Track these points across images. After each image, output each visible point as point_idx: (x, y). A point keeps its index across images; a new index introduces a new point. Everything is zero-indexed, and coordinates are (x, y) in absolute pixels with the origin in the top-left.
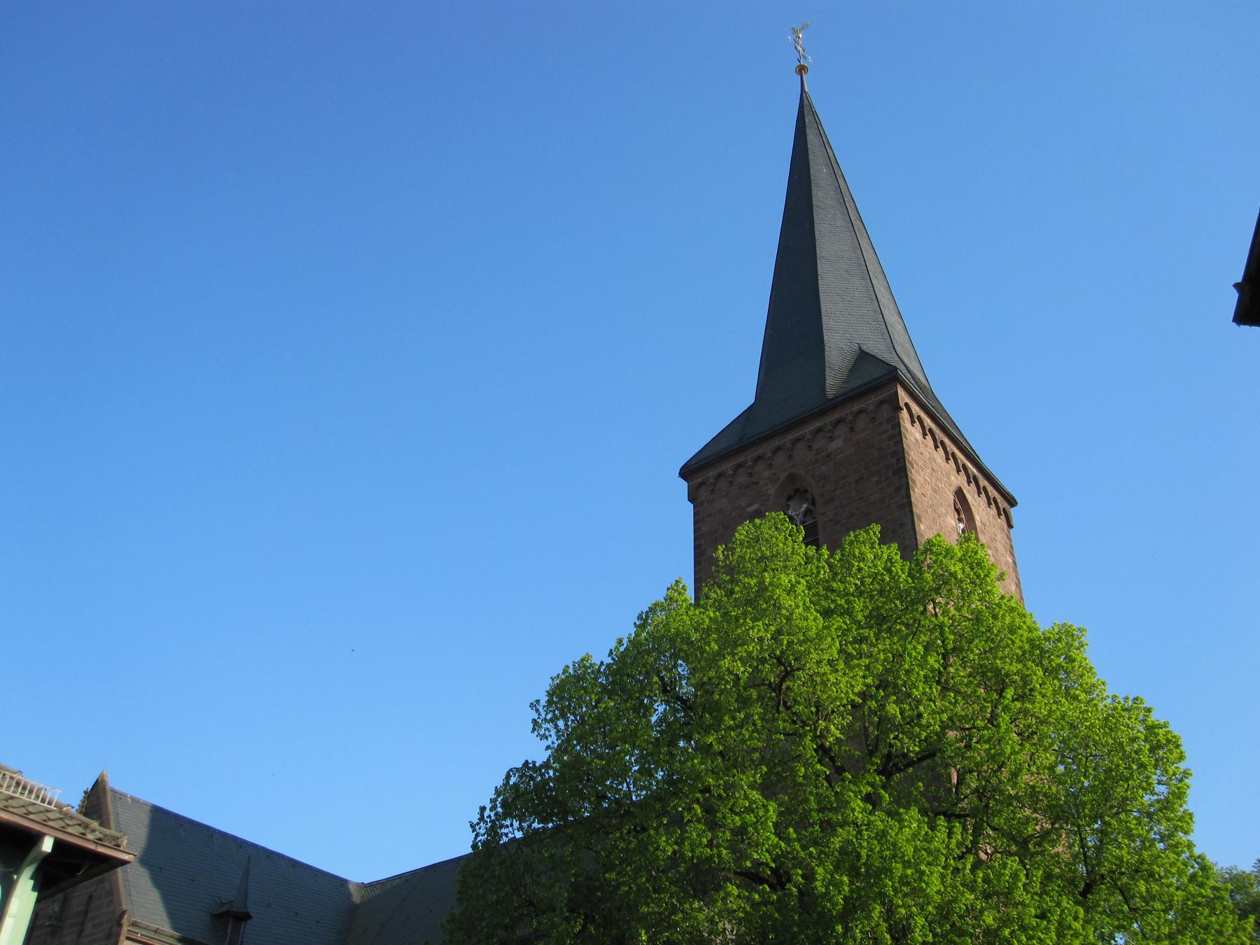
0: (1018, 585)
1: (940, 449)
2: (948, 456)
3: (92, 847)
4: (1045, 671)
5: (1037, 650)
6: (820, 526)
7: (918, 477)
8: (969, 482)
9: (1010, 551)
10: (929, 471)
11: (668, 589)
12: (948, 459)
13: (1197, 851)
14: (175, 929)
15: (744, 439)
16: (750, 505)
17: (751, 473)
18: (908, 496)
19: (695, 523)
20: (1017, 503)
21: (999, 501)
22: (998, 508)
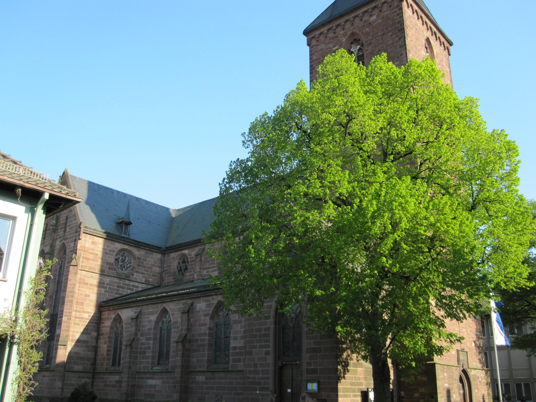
0: (451, 81)
1: (420, 20)
3: (65, 196)
4: (461, 117)
5: (457, 108)
6: (365, 56)
7: (409, 33)
10: (414, 30)
11: (298, 84)
12: (423, 24)
13: (519, 193)
14: (102, 228)
16: (334, 47)
17: (335, 32)
18: (405, 41)
19: (310, 55)
22: (444, 46)
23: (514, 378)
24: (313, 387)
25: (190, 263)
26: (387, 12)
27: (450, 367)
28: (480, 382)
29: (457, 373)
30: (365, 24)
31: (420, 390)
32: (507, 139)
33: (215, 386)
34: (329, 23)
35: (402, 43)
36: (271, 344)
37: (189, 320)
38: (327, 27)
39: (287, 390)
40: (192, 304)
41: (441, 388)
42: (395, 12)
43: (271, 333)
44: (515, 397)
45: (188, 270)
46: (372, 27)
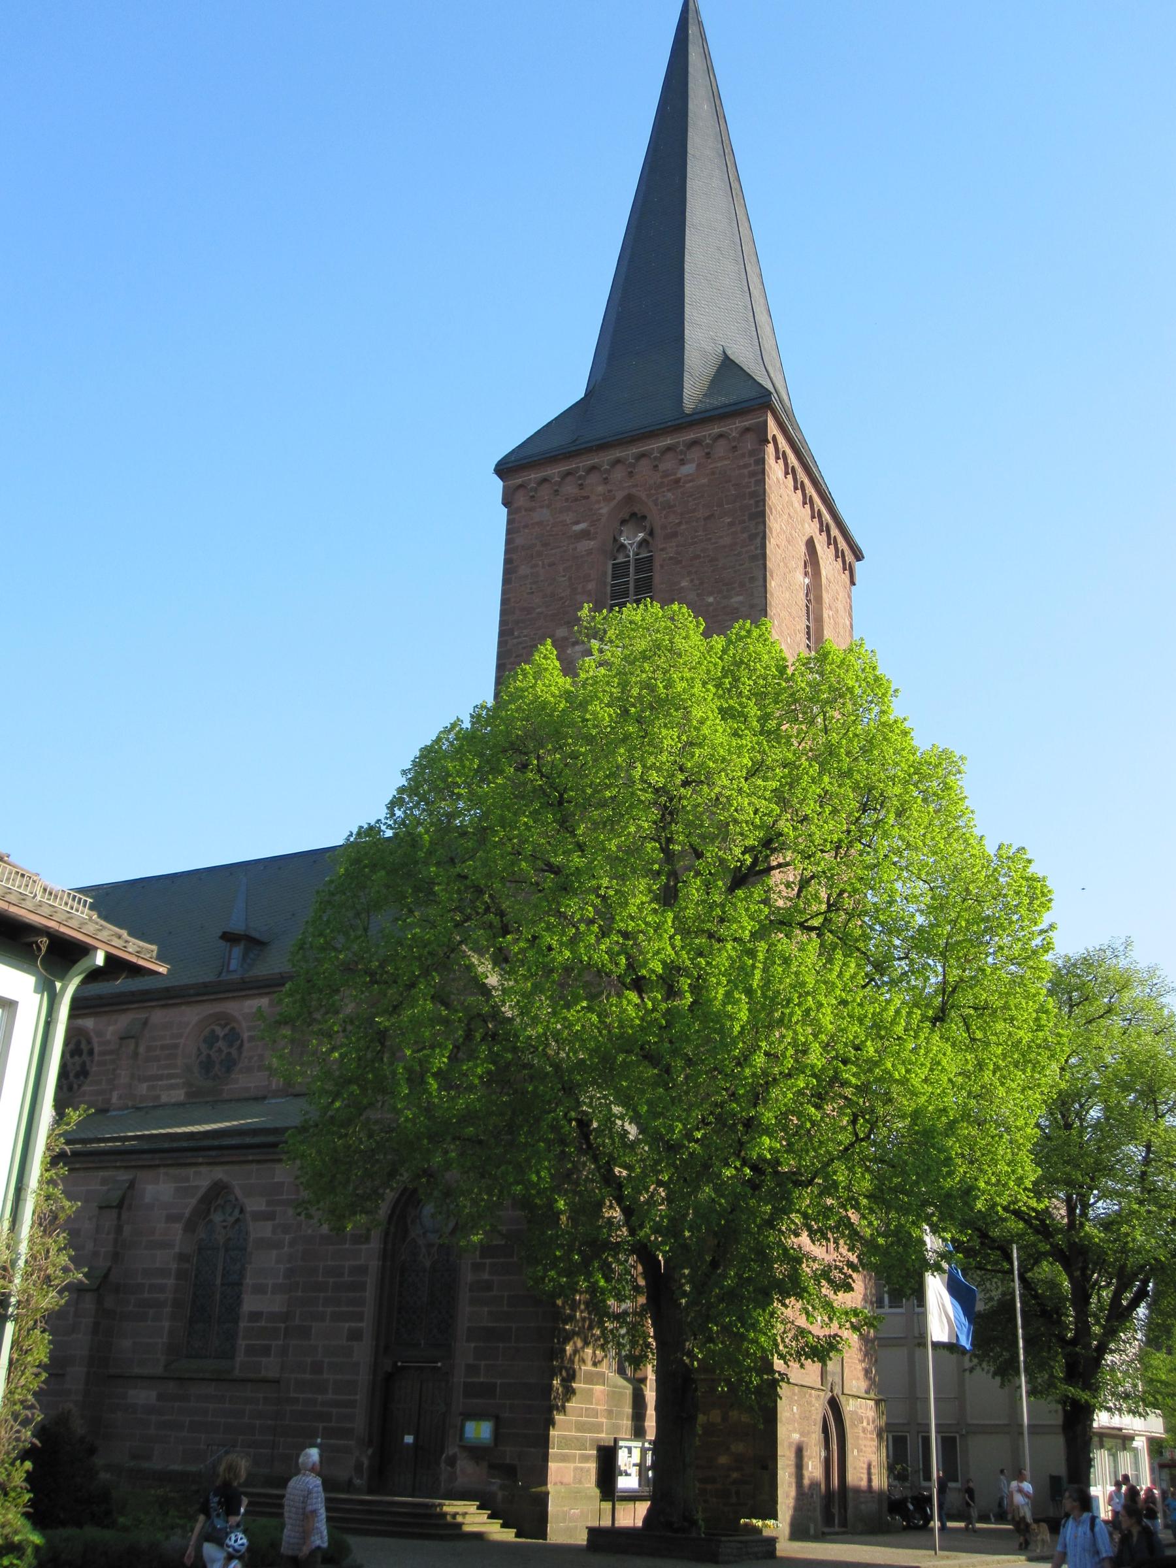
2: (807, 501)
3: (134, 959)
5: (919, 772)
6: (657, 564)
8: (821, 531)
10: (786, 517)
12: (804, 503)
15: (577, 442)
16: (577, 523)
18: (763, 547)
19: (509, 532)
21: (846, 553)
23: (920, 1422)
24: (480, 1431)
25: (96, 1058)
26: (726, 462)
27: (805, 1389)
28: (864, 1430)
29: (818, 1406)
30: (666, 480)
31: (733, 1448)
32: (1032, 870)
34: (570, 457)
35: (756, 548)
36: (369, 1310)
37: (119, 1229)
38: (563, 468)
39: (403, 1439)
40: (132, 1184)
41: (786, 1444)
42: (745, 466)
43: (371, 1281)
44: (919, 1471)
45: (90, 1079)
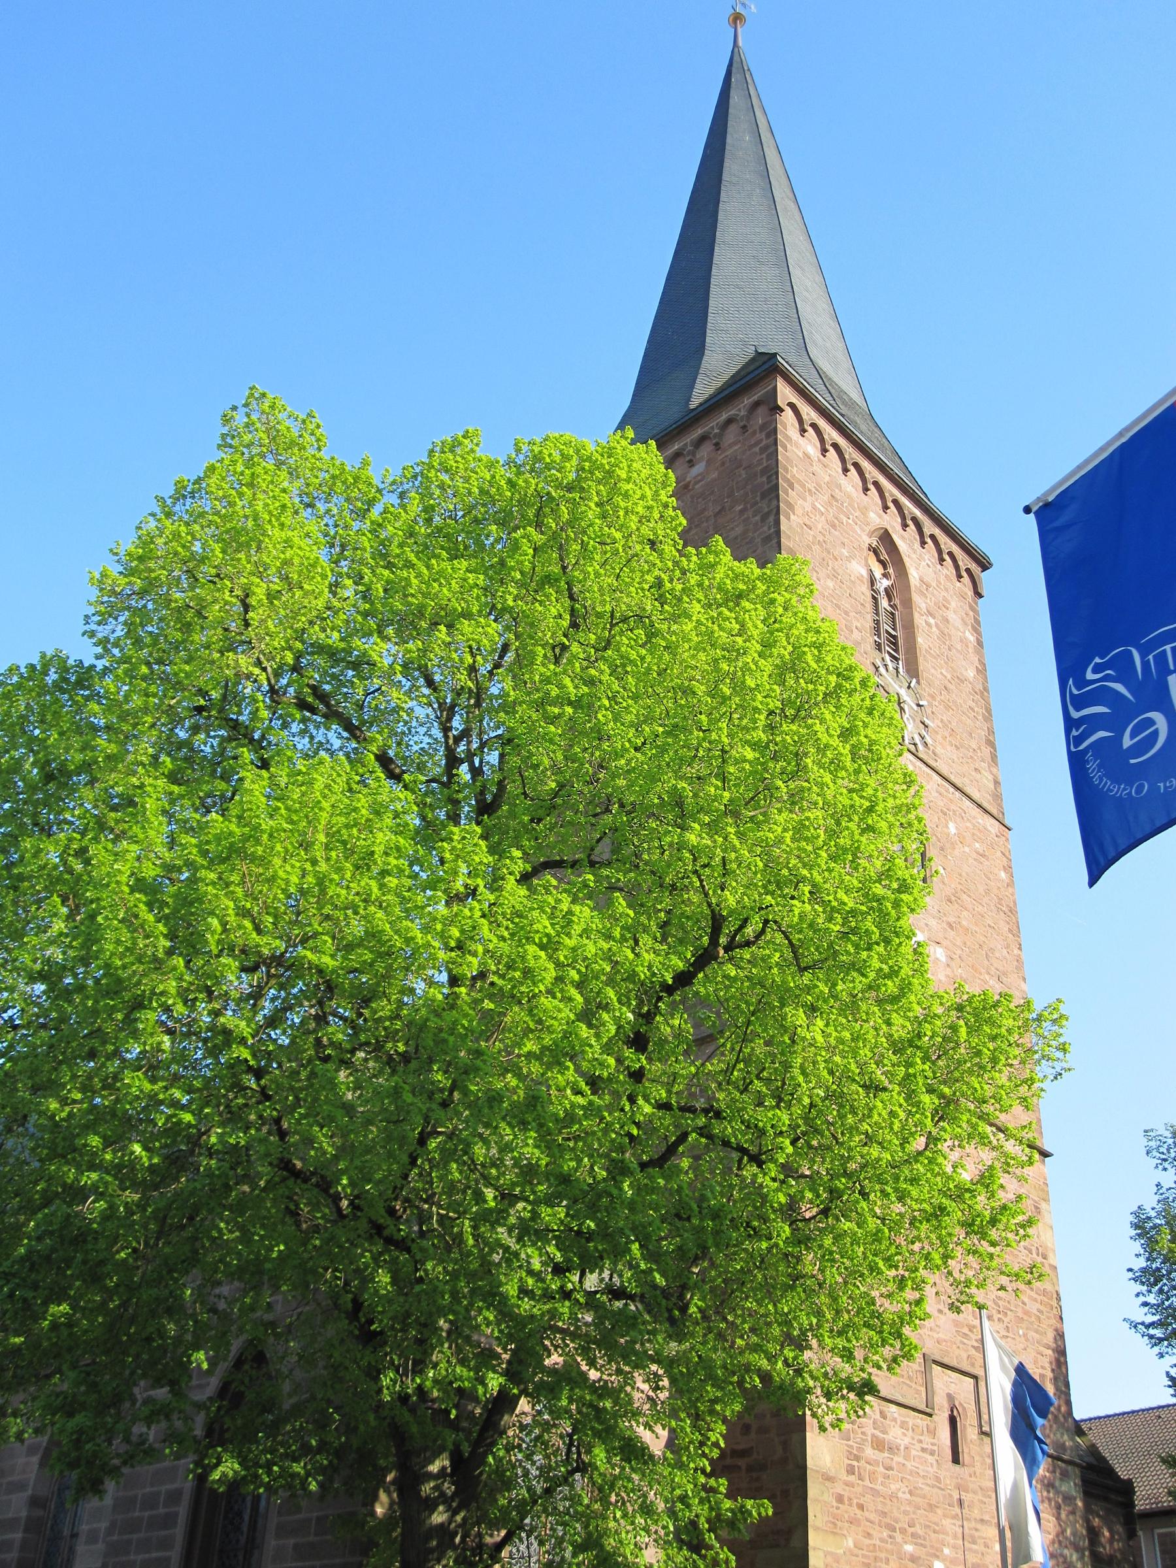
9: (973, 627)
18: (777, 523)
20: (991, 565)
33: (273, 1543)
35: (769, 528)
42: (756, 444)
46: (692, 497)
